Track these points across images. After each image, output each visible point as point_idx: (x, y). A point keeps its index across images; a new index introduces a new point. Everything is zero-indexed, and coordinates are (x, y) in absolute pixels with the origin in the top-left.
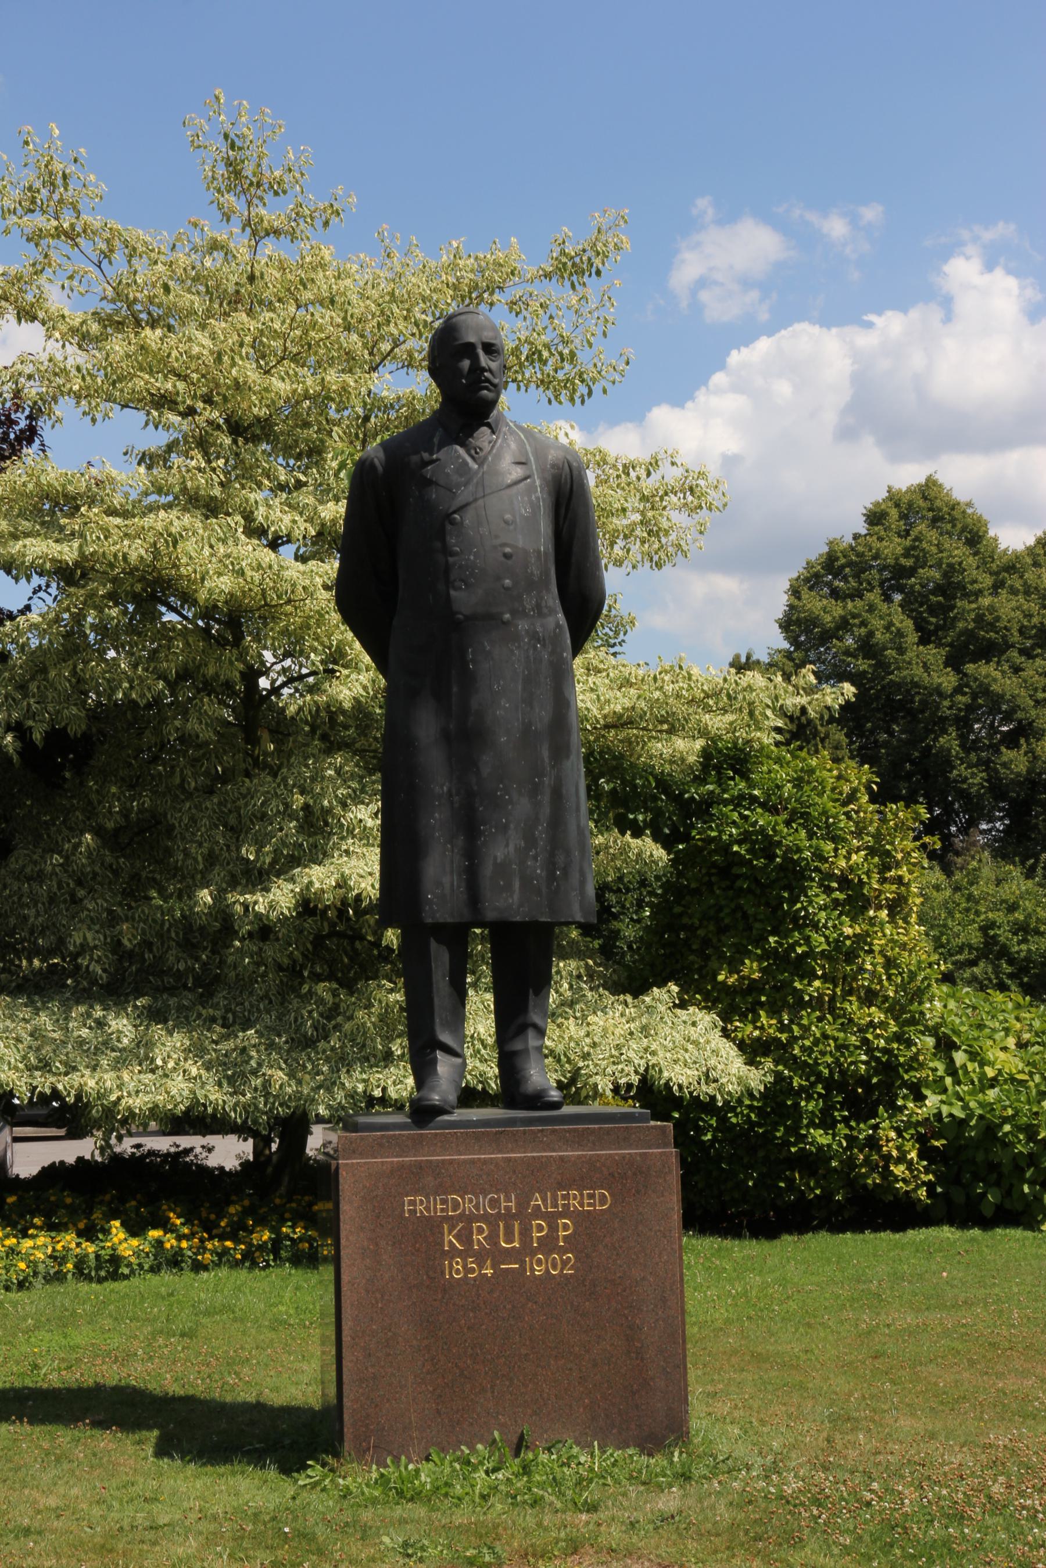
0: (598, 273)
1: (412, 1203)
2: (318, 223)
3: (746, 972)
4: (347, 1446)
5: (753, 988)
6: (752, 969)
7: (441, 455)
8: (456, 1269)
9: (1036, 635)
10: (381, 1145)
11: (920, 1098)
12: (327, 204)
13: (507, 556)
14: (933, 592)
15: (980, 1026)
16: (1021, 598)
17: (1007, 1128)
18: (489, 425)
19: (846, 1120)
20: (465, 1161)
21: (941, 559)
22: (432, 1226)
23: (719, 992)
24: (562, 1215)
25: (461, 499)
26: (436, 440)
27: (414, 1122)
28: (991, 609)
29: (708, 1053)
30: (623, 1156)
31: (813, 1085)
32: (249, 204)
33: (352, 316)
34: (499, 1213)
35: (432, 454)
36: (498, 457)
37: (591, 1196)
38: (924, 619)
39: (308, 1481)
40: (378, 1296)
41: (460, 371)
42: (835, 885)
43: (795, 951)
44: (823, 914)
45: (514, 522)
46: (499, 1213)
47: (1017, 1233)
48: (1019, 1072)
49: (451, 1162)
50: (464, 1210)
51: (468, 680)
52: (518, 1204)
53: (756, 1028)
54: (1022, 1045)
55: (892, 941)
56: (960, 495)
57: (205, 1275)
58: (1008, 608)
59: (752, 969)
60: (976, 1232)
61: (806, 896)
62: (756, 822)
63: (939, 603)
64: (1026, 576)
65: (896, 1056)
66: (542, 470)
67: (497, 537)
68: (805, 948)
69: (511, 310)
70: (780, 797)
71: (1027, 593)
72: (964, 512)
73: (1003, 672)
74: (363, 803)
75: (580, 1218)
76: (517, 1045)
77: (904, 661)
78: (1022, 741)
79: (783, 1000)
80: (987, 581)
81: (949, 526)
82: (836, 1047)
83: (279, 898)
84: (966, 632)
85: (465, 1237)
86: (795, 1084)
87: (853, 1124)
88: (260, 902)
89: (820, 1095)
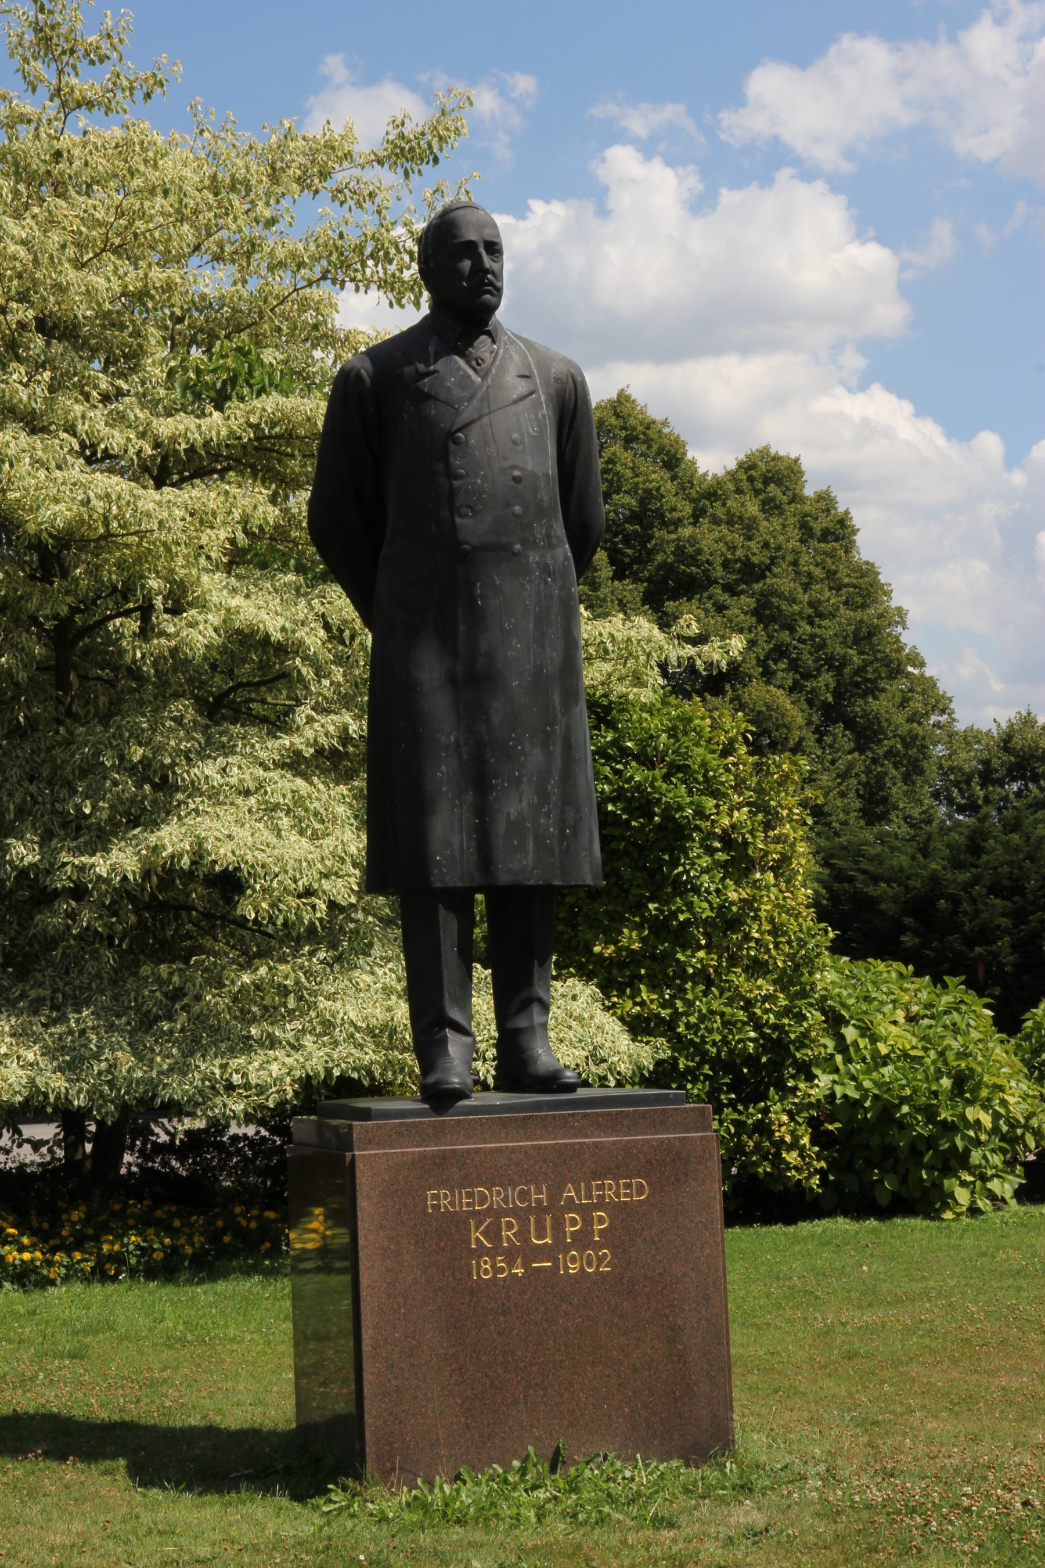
0: (436, 160)
1: (435, 1197)
2: (139, 95)
3: (624, 942)
4: (369, 1466)
5: (633, 959)
6: (631, 939)
7: (440, 366)
8: (484, 1269)
9: (739, 571)
10: (400, 1134)
11: (810, 1077)
12: (149, 73)
13: (517, 480)
14: (628, 520)
15: (867, 999)
16: (724, 528)
17: (905, 1109)
18: (489, 334)
19: (732, 1104)
20: (492, 1150)
21: (637, 484)
22: (458, 1222)
23: (595, 964)
24: (597, 1207)
25: (465, 417)
26: (431, 349)
27: (432, 1108)
28: (693, 540)
29: (593, 1030)
30: (661, 1142)
31: (700, 1065)
32: (60, 72)
33: (186, 207)
34: (530, 1206)
35: (428, 365)
36: (502, 369)
37: (628, 1186)
38: (620, 551)
39: (332, 1507)
40: (400, 1300)
41: (460, 272)
42: (717, 845)
43: (676, 918)
44: (706, 877)
45: (522, 442)
46: (530, 1206)
47: (917, 1222)
48: (913, 1048)
49: (477, 1151)
50: (492, 1204)
51: (476, 617)
52: (550, 1197)
53: (635, 1004)
54: (911, 1019)
55: (778, 906)
56: (655, 413)
57: (51, 1290)
58: (710, 539)
59: (631, 939)
60: (872, 1223)
61: (687, 857)
62: (632, 778)
63: (635, 531)
64: (729, 503)
65: (787, 1033)
66: (546, 384)
67: (505, 458)
68: (687, 915)
69: (334, 198)
70: (656, 748)
71: (730, 523)
72: (660, 431)
73: (706, 610)
74: (210, 757)
75: (617, 1210)
76: (521, 1022)
77: (598, 598)
78: (728, 687)
79: (664, 974)
80: (688, 509)
81: (644, 447)
82: (722, 1023)
83: (120, 861)
84: (664, 565)
85: (494, 1234)
86: (681, 1066)
87: (740, 1108)
88: (101, 865)
89: (706, 1076)
